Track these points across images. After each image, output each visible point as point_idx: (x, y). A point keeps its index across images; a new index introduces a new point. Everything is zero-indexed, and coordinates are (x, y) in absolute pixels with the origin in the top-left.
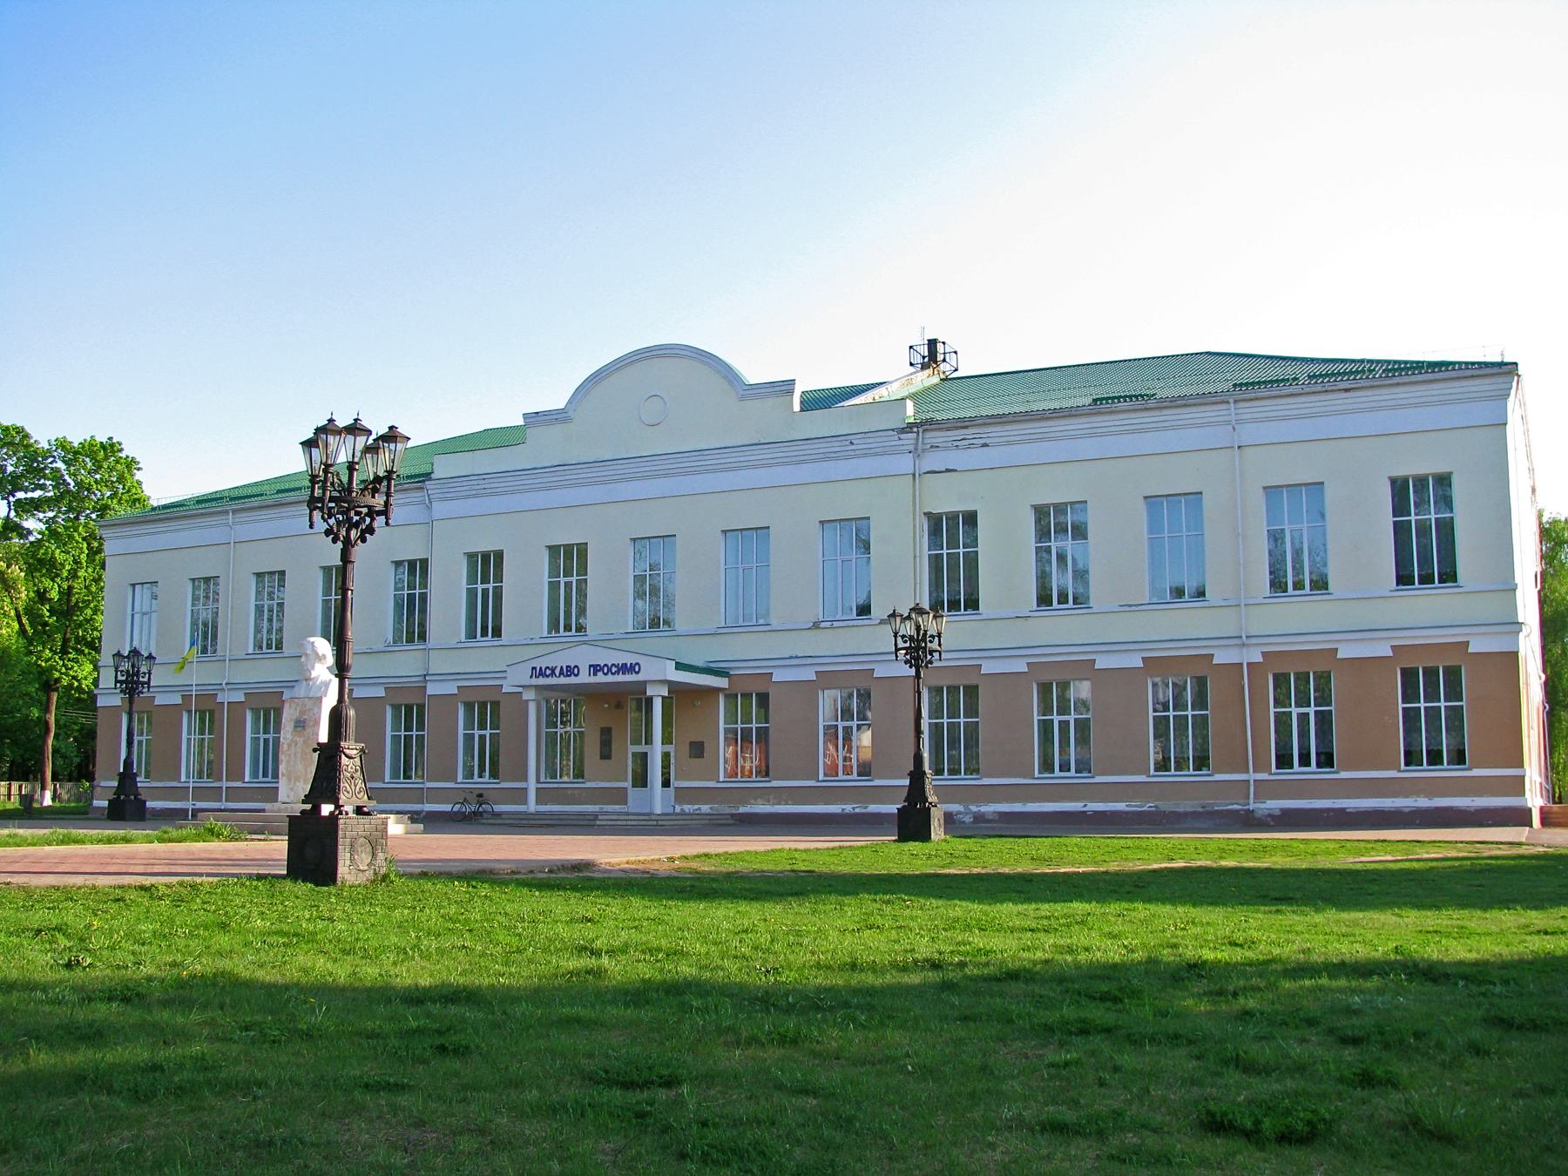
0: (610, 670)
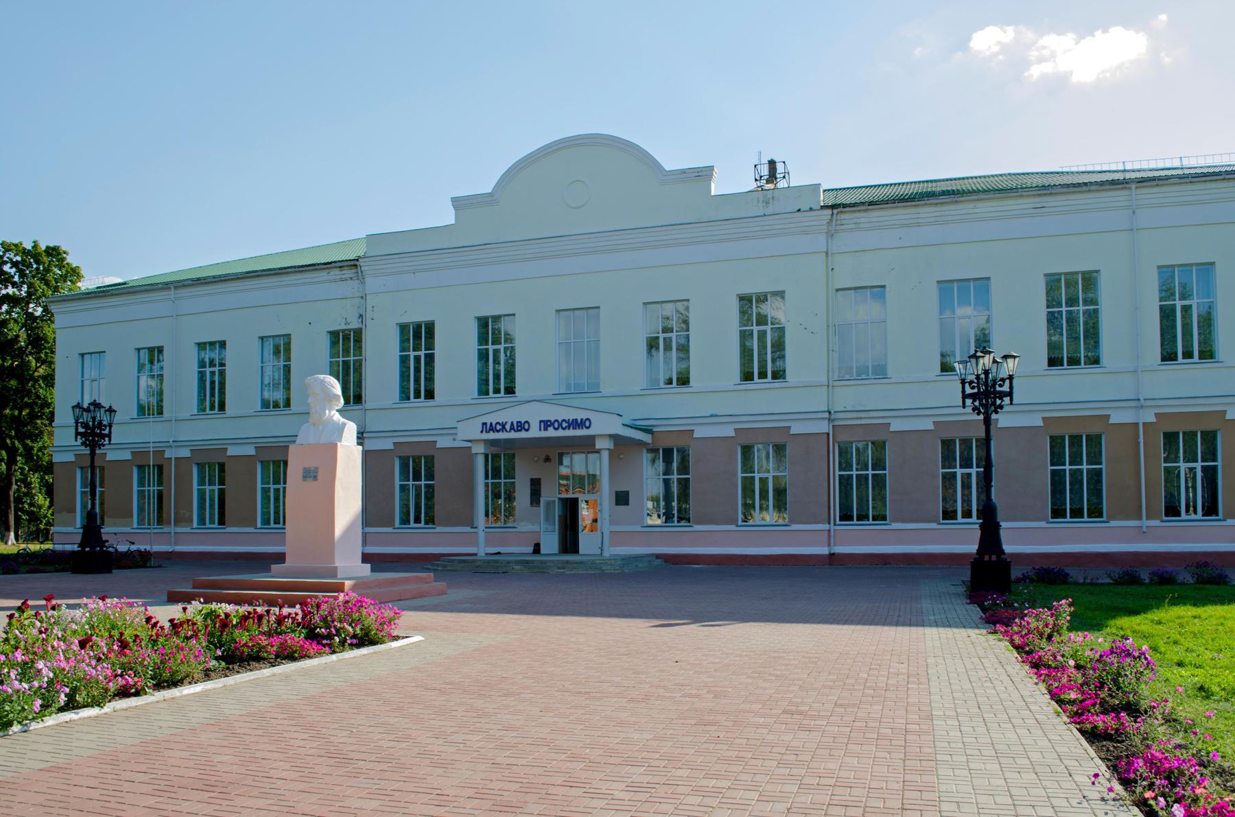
0: (560, 425)
